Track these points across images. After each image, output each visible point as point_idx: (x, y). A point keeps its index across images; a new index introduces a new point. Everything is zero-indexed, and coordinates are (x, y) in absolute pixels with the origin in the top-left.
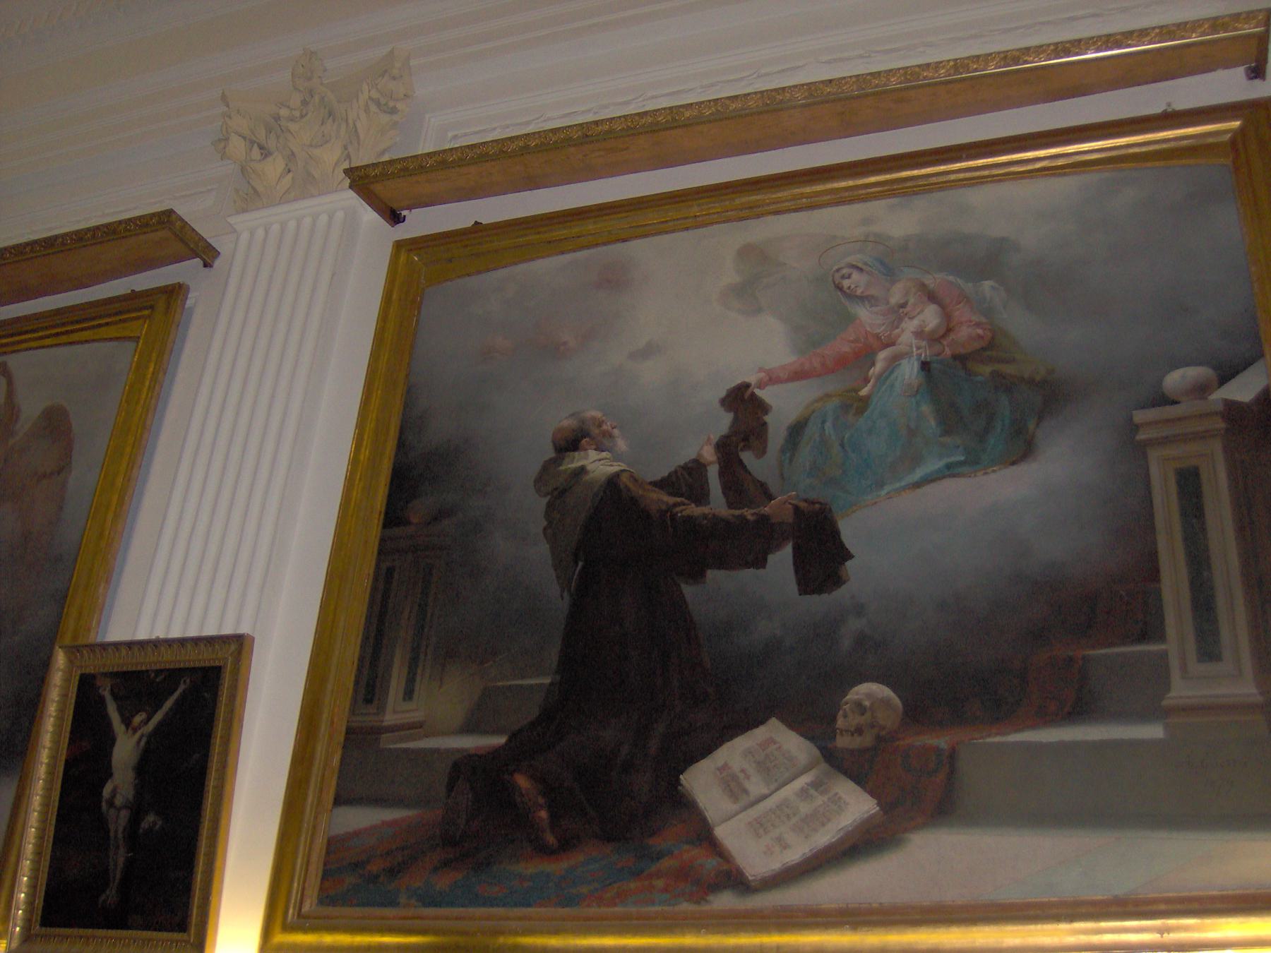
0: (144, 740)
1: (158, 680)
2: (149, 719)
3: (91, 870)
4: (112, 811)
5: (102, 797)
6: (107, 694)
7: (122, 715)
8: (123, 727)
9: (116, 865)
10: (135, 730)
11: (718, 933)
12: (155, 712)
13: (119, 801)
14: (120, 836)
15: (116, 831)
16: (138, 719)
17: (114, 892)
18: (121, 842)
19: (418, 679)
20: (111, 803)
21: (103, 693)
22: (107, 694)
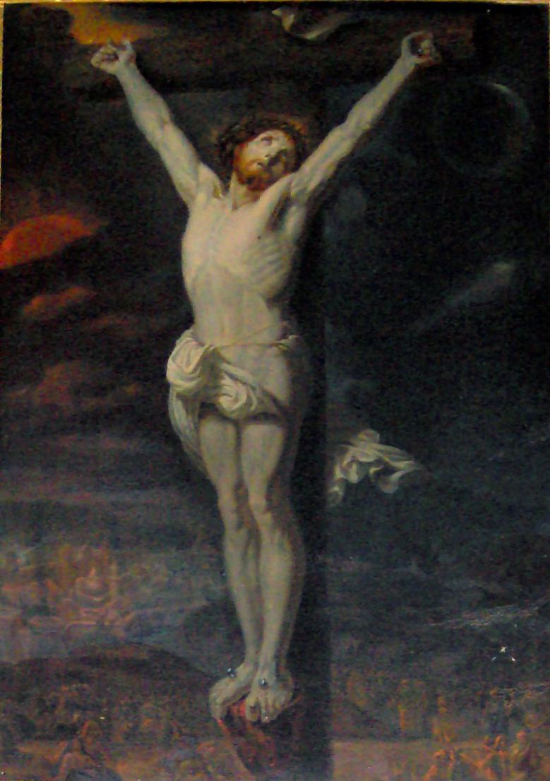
0: (294, 221)
1: (311, 36)
2: (298, 157)
3: (15, 373)
4: (211, 430)
5: (166, 386)
6: (123, 70)
7: (193, 136)
8: (206, 173)
9: (257, 594)
10: (256, 185)
11: (307, 222)
12: (321, 134)
13: (232, 397)
14: (257, 499)
15: (240, 489)
16: (258, 151)
17: (265, 675)
18: (264, 520)
19: (221, 94)
20: (205, 406)
21: (110, 68)
22: (123, 70)
